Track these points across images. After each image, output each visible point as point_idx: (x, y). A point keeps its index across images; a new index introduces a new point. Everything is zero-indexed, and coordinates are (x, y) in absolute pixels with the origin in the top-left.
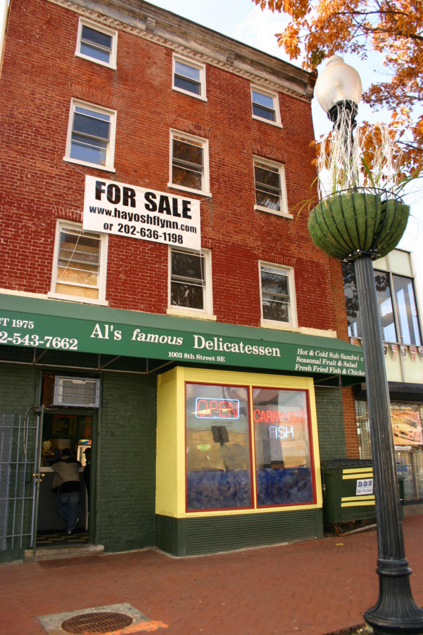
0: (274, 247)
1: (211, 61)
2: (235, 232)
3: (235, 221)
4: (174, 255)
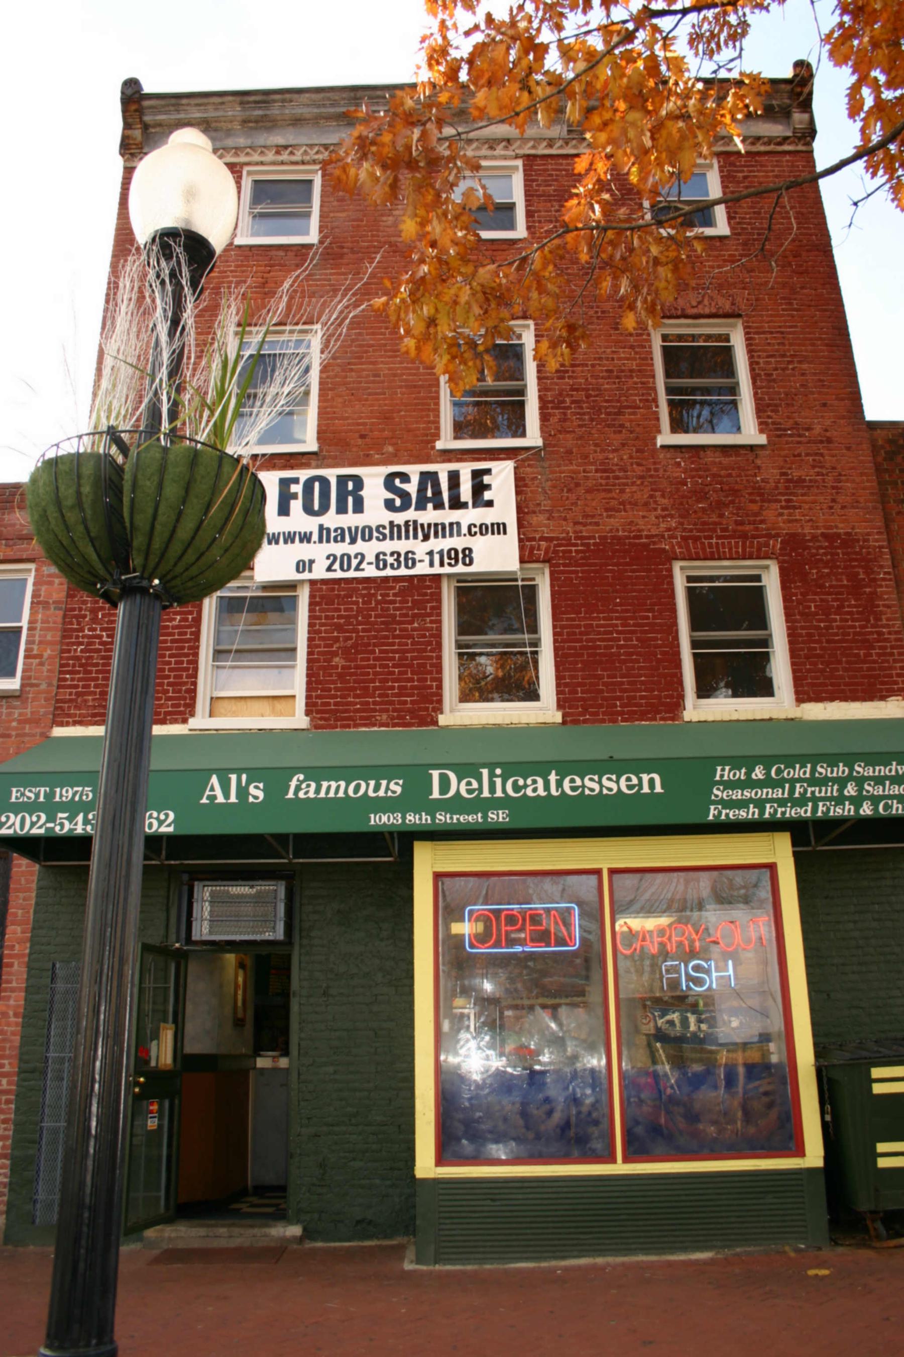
0: (715, 523)
1: (534, 147)
2: (607, 510)
3: (607, 484)
4: (461, 592)
